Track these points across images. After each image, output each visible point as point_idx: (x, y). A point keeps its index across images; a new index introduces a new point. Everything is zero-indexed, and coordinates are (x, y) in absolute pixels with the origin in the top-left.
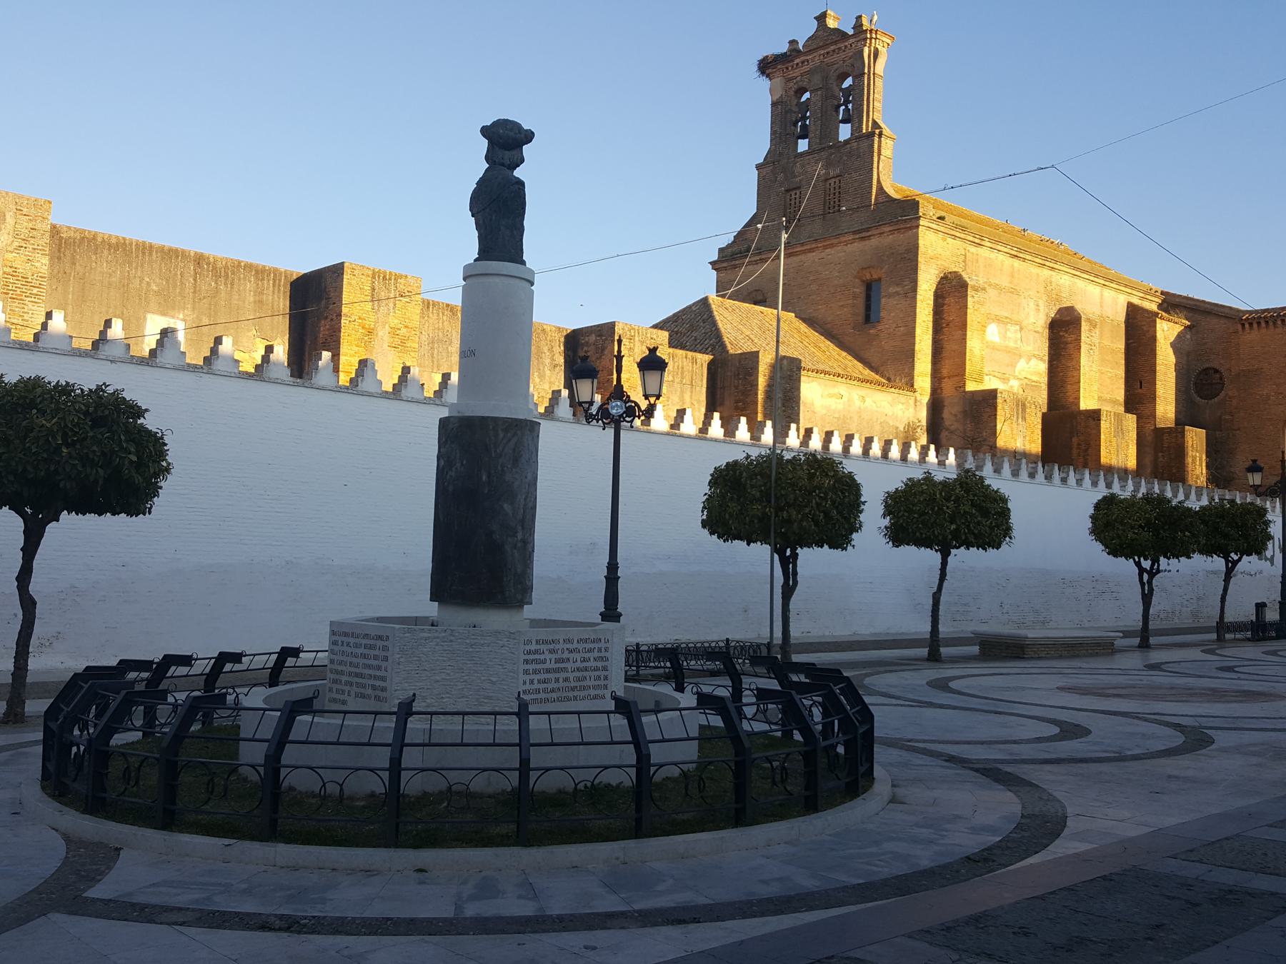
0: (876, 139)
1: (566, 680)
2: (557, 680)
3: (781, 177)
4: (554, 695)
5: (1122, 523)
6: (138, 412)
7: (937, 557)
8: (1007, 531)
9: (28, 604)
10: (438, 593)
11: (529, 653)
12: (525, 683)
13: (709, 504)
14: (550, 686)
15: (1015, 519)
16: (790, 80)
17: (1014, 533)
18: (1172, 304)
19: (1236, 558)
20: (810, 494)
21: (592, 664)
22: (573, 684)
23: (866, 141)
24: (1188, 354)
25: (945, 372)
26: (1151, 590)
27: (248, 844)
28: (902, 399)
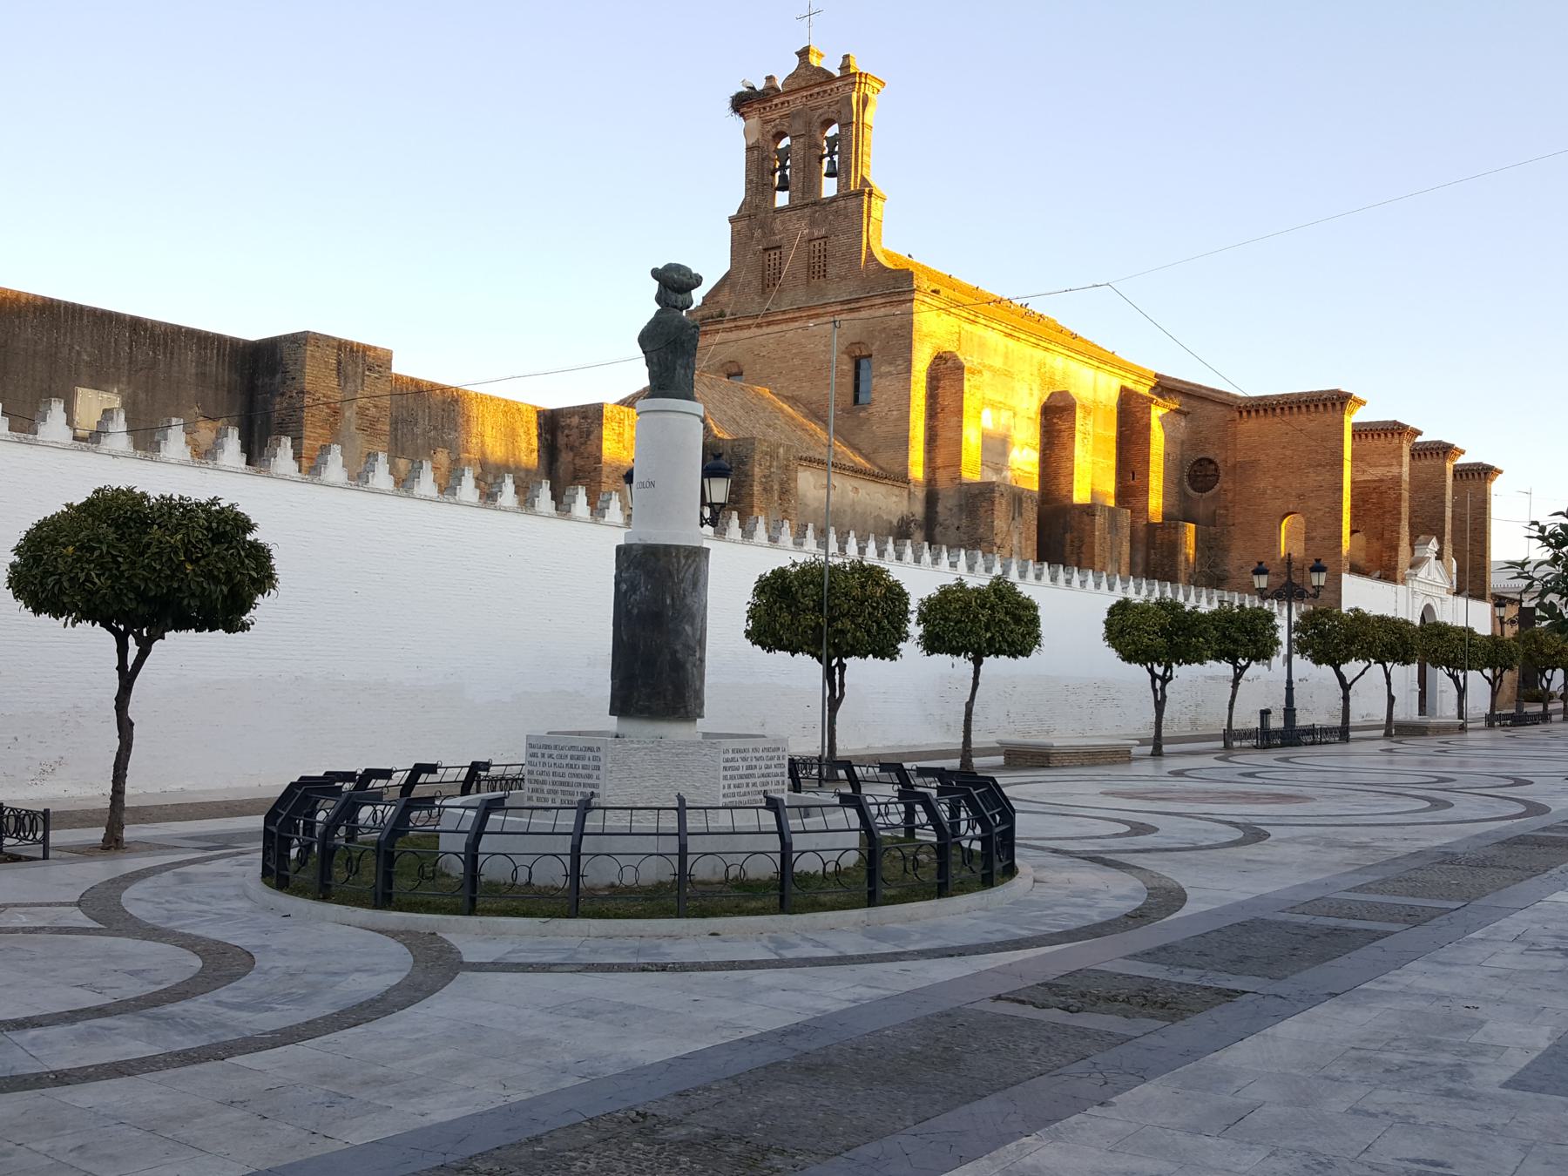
0: (866, 198)
3: (758, 233)
5: (1137, 629)
6: (248, 526)
7: (971, 665)
8: (1037, 638)
9: (125, 728)
13: (753, 614)
15: (1044, 629)
16: (766, 122)
17: (1043, 641)
18: (1165, 387)
19: (1244, 663)
20: (862, 603)
21: (773, 770)
23: (857, 196)
24: (1183, 443)
25: (939, 462)
26: (1164, 697)
27: (557, 921)
28: (896, 491)
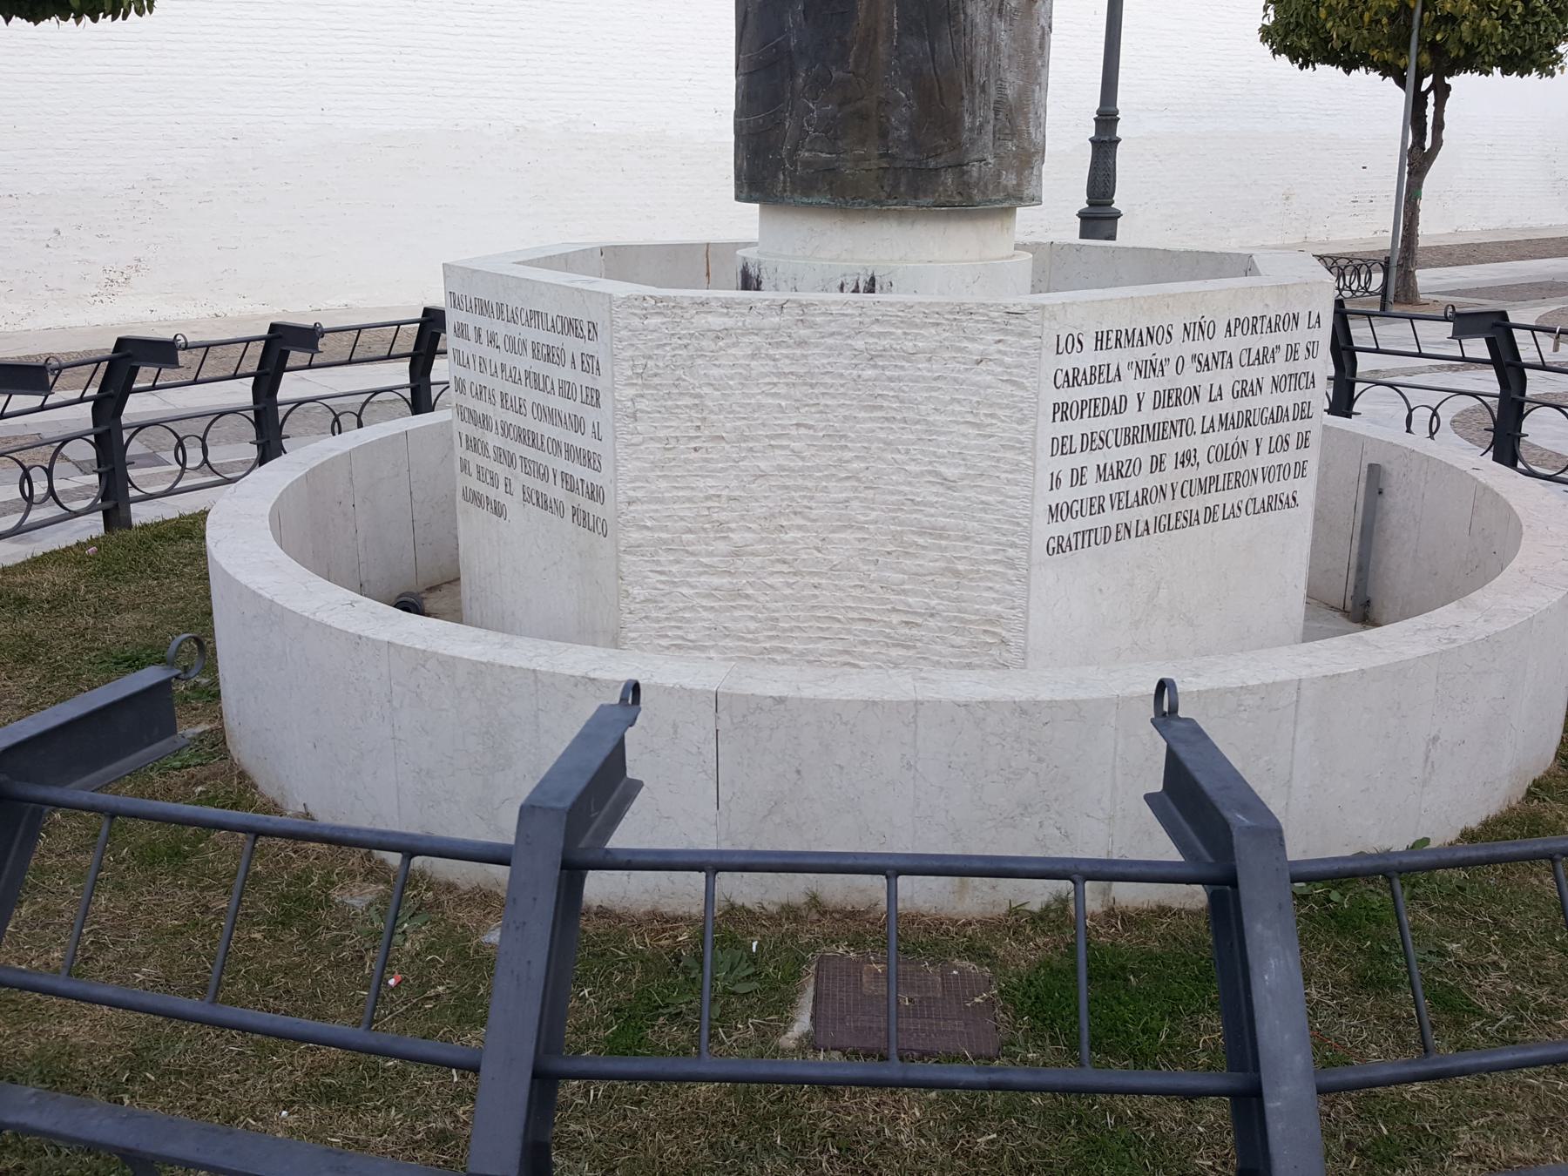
1: (1185, 459)
2: (1158, 463)
4: (1147, 513)
10: (763, 171)
11: (1072, 379)
12: (1056, 482)
14: (1133, 485)
22: (1206, 471)
